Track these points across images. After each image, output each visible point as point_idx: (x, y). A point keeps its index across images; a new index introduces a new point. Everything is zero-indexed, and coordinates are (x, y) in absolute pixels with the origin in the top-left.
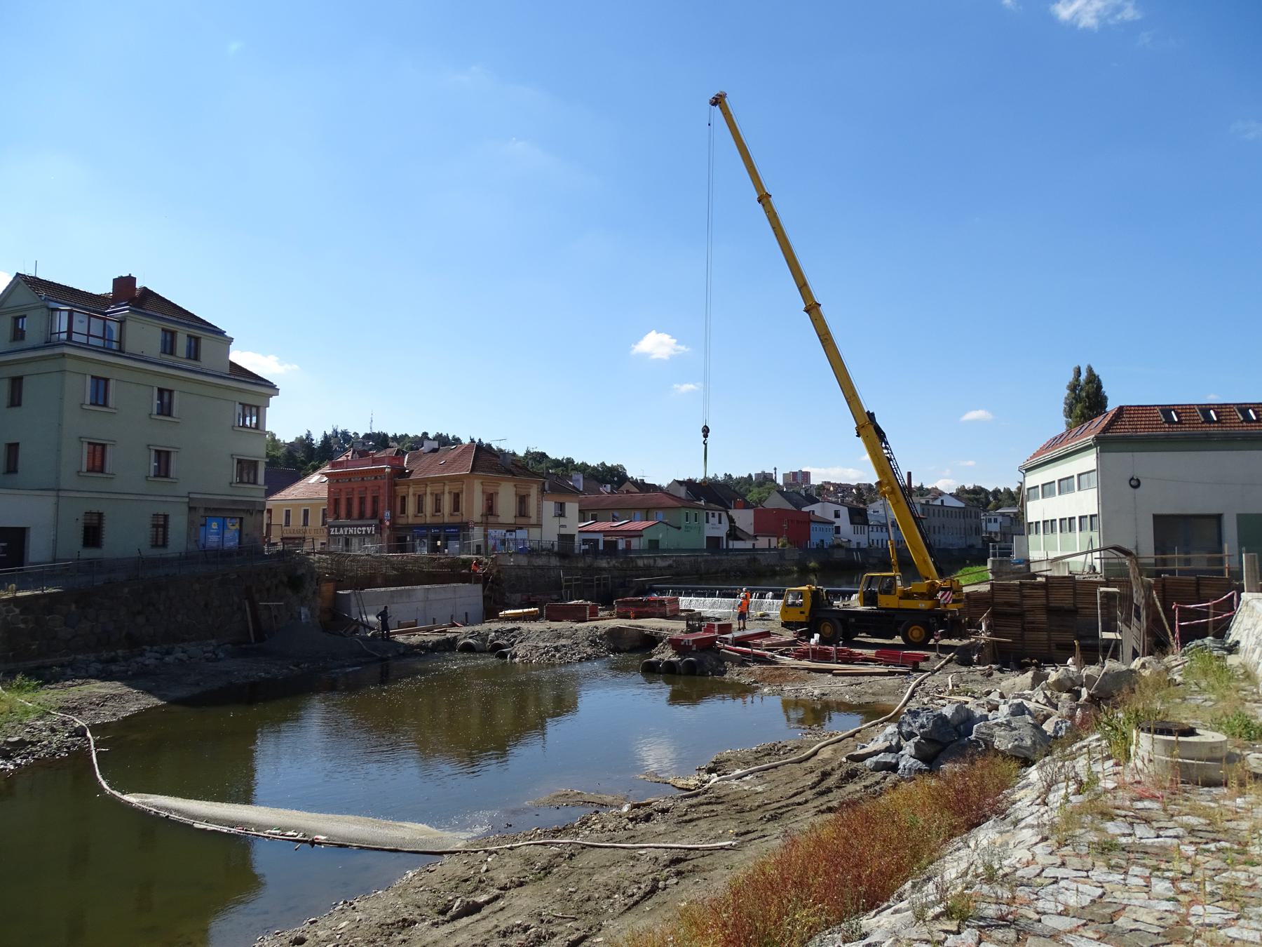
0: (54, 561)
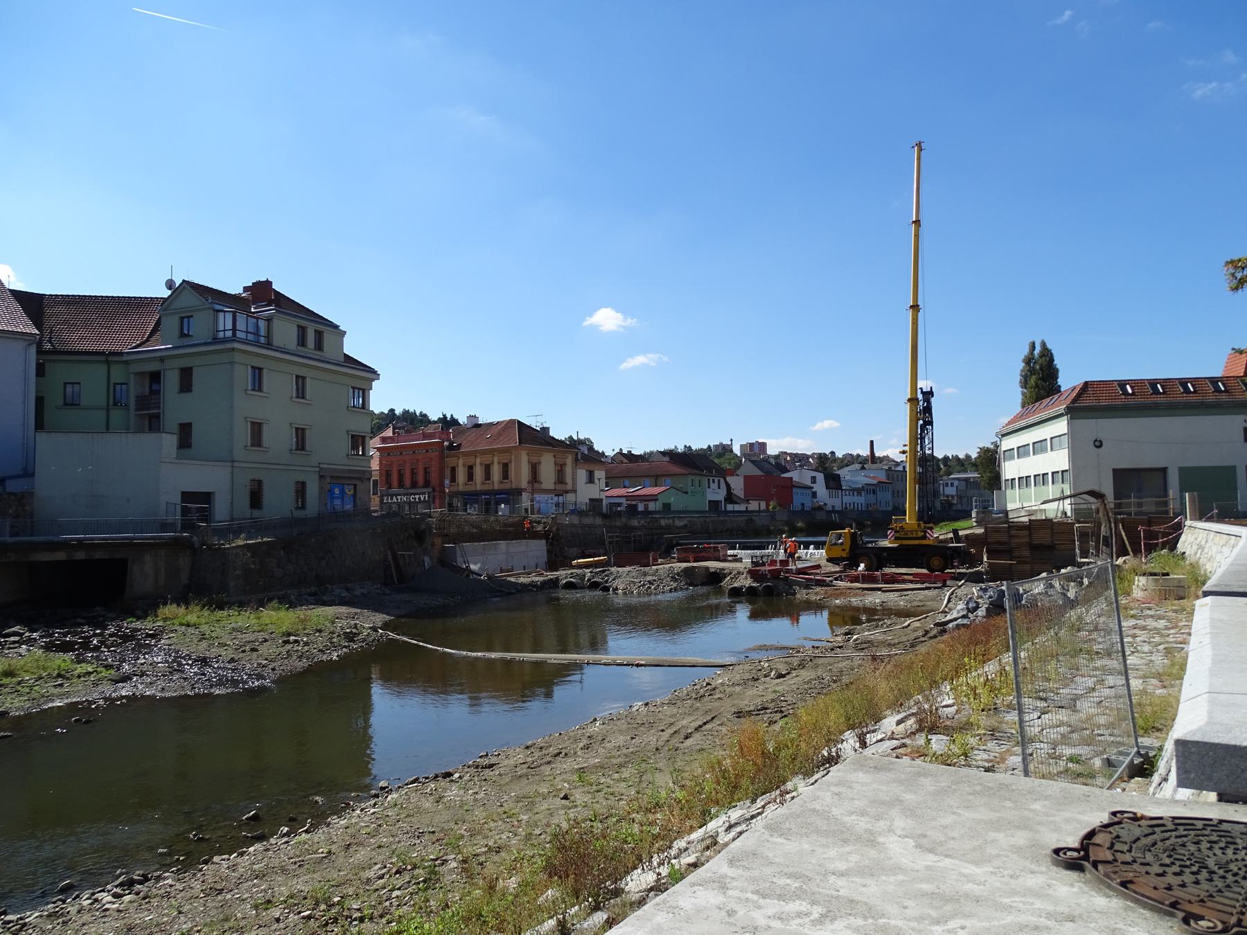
0: (232, 520)
